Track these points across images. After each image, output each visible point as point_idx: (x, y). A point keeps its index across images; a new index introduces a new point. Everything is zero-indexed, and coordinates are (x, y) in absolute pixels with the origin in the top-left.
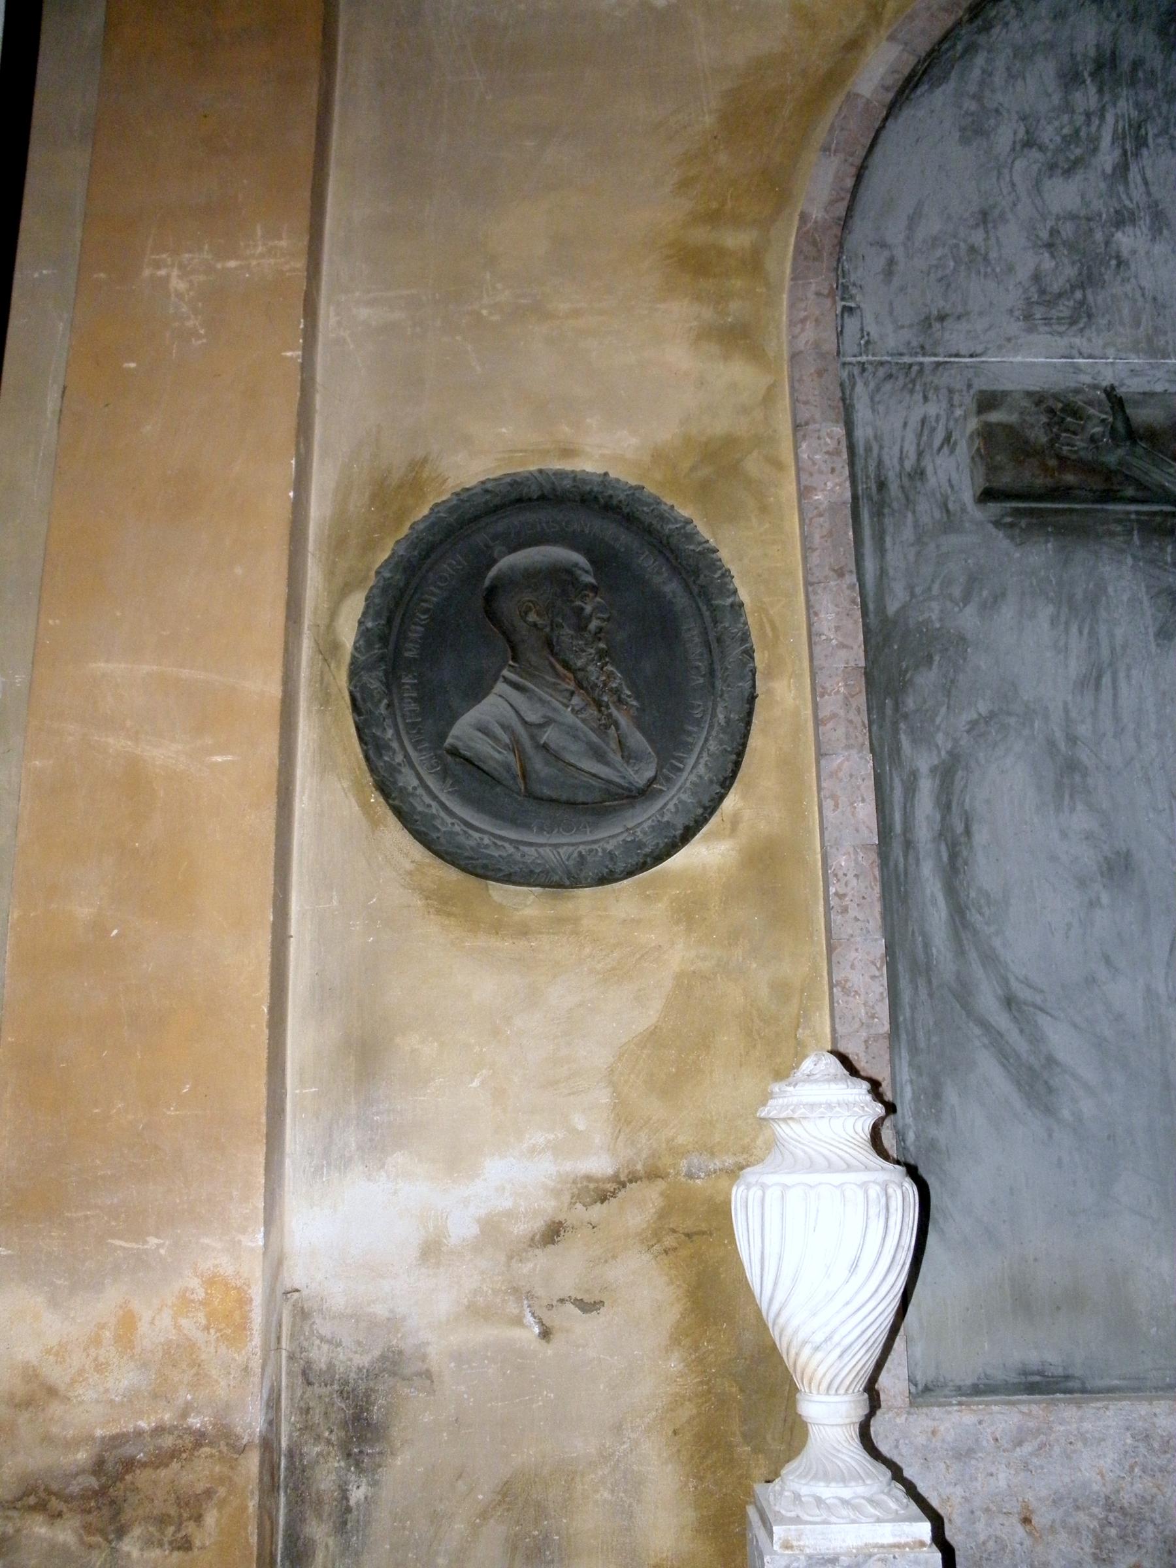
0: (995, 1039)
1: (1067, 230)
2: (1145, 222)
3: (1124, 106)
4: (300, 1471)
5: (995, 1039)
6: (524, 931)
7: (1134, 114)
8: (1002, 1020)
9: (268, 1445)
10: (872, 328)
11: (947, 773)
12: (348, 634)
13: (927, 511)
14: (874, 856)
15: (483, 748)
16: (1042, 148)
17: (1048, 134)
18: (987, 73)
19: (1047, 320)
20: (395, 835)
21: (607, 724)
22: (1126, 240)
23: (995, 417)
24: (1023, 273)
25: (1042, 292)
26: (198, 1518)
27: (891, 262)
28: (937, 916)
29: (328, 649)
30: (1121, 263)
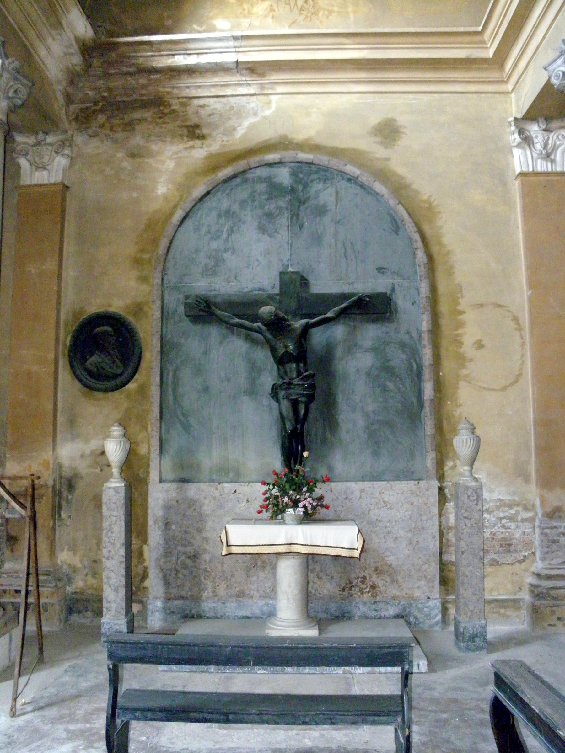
0: (180, 420)
1: (214, 253)
2: (230, 251)
3: (230, 223)
4: (60, 493)
5: (180, 420)
6: (99, 400)
7: (232, 225)
8: (181, 417)
9: (54, 487)
10: (170, 278)
11: (175, 371)
12: (68, 343)
13: (177, 318)
14: (159, 387)
15: (90, 367)
16: (211, 234)
17: (213, 230)
18: (202, 215)
19: (207, 275)
20: (77, 383)
21: (114, 362)
22: (225, 255)
23: (188, 301)
24: (203, 264)
25: (206, 268)
26: (42, 498)
27: (176, 262)
28: (171, 398)
29: (65, 345)
30: (224, 261)
